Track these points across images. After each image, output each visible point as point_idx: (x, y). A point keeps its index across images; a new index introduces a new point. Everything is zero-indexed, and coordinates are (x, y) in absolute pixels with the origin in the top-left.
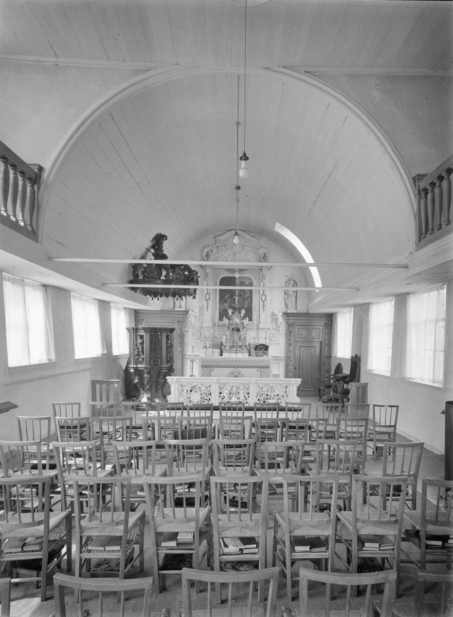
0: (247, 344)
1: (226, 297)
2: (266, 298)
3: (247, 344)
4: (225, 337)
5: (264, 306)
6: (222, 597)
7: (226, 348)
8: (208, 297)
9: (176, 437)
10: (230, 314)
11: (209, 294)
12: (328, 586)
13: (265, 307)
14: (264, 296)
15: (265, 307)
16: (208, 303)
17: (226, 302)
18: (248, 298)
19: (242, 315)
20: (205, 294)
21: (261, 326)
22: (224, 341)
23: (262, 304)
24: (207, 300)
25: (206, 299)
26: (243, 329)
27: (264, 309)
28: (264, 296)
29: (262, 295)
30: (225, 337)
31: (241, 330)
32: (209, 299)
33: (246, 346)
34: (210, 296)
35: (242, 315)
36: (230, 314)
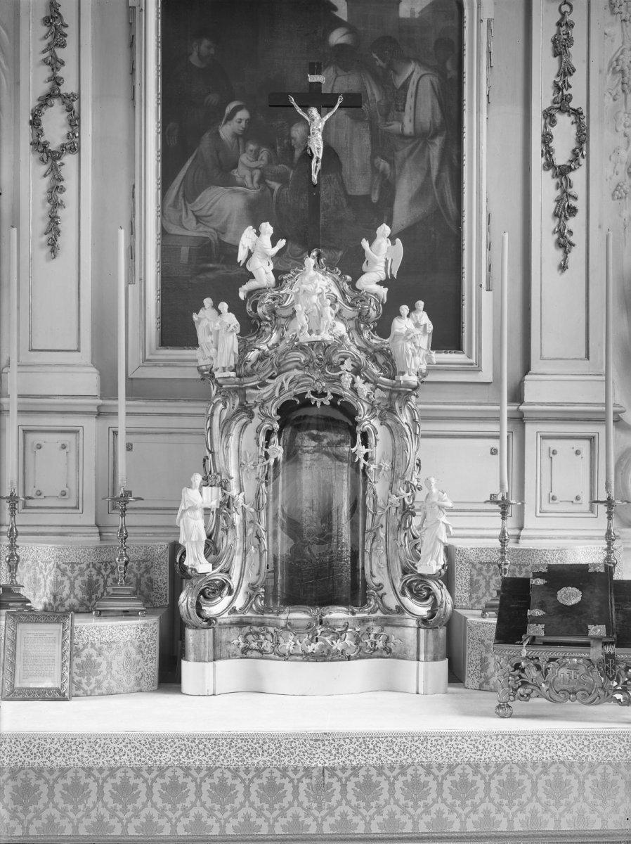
0: (431, 564)
1: (227, 131)
2: (582, 138)
3: (431, 564)
4: (210, 497)
5: (565, 210)
6: (335, 88)
7: (217, 608)
8: (55, 127)
9: (615, 413)
10: (263, 272)
11: (71, 104)
12: (115, 402)
13: (574, 223)
14: (564, 121)
15: (626, 86)
16: (56, 188)
17: (223, 172)
18: (422, 137)
19: (371, 282)
20: (29, 102)
21: (536, 393)
22: (193, 531)
23: (545, 189)
24: (50, 156)
25: (40, 146)
26: (387, 412)
27: (564, 244)
28: (564, 121)
29: (549, 116)
30: (210, 497)
31: (367, 421)
32: (73, 146)
33: (418, 587)
34: (74, 121)
35: (371, 282)
36: (263, 272)
